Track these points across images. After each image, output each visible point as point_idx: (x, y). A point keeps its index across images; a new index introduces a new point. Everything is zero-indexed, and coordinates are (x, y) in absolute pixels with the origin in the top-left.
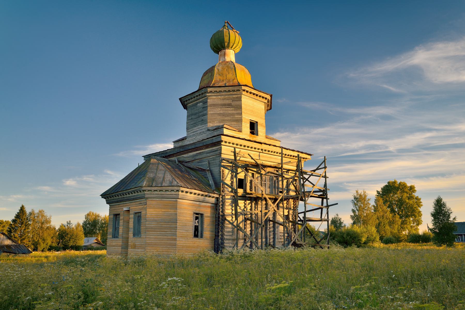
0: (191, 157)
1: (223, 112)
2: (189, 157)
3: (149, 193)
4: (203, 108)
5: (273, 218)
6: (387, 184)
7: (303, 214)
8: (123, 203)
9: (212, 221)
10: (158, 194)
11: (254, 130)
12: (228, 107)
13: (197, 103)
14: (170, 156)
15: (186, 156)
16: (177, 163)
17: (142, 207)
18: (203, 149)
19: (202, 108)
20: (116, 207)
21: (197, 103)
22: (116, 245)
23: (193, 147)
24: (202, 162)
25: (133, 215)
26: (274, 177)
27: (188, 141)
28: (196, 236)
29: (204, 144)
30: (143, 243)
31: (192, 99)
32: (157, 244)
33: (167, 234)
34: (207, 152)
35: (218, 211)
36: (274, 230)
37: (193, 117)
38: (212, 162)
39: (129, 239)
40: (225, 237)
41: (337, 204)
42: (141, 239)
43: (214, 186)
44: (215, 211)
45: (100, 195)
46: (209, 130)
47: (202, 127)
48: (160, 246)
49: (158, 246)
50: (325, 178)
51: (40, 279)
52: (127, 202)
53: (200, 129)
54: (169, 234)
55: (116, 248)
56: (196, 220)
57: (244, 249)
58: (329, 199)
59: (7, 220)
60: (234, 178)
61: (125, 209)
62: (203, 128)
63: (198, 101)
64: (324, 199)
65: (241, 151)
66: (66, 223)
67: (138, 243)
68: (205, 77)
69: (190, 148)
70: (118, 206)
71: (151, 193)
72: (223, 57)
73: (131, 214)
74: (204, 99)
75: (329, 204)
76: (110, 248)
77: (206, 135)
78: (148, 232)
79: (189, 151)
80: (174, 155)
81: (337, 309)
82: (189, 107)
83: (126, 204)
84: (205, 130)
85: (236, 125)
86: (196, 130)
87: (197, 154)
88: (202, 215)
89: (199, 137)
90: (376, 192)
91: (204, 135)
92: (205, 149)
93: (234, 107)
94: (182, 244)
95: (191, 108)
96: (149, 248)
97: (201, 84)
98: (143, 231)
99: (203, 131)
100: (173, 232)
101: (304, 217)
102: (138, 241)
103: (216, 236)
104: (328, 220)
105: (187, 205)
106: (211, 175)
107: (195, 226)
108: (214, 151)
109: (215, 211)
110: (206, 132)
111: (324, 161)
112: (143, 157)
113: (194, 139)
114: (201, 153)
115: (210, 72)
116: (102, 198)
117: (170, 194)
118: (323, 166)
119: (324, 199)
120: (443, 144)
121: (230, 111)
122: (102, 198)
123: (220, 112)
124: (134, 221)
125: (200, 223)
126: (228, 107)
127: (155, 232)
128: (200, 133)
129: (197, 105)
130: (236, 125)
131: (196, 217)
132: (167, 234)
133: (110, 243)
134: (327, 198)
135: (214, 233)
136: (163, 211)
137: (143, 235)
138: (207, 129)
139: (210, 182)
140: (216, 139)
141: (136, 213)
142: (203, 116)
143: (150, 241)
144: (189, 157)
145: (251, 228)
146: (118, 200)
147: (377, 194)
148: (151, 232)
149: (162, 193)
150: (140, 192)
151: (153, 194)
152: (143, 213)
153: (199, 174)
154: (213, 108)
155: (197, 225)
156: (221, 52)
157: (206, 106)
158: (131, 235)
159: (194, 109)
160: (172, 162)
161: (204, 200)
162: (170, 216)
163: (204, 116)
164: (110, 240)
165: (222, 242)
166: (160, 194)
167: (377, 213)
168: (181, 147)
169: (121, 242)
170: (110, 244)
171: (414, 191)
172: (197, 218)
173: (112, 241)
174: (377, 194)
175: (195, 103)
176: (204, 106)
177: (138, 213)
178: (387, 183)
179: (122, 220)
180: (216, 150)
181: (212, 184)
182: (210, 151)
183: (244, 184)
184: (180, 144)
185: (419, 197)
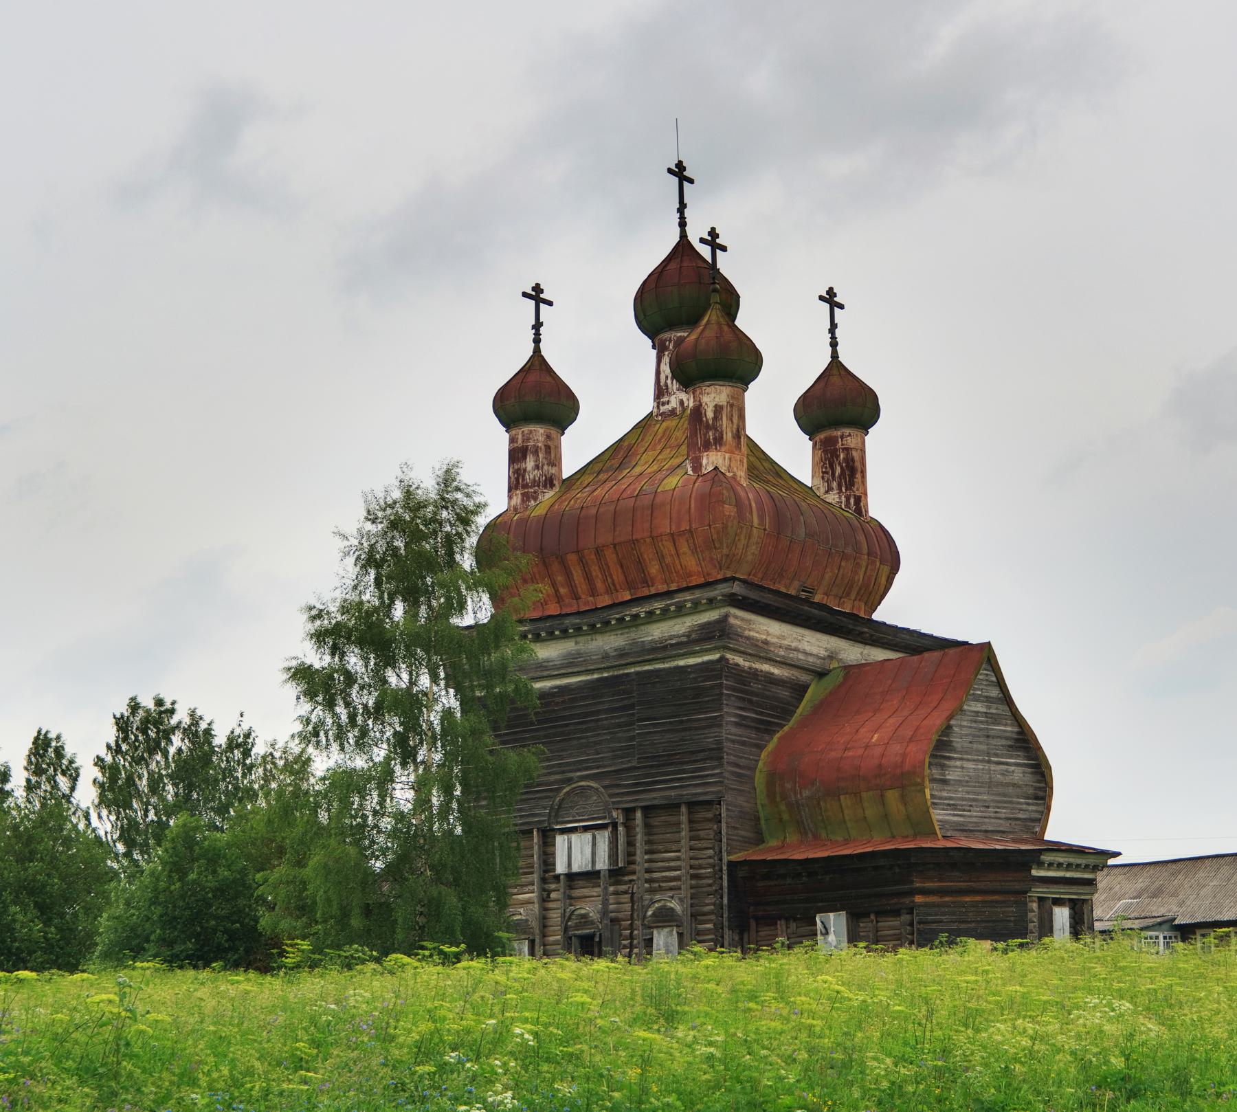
51: (672, 987)
57: (300, 1104)
59: (835, 291)
60: (769, 845)
66: (96, 769)
81: (667, 1111)
82: (548, 437)
90: (292, 690)
105: (575, 898)
114: (770, 722)
120: (924, 846)
121: (1042, 785)
127: (1074, 889)
167: (152, 816)
185: (123, 709)
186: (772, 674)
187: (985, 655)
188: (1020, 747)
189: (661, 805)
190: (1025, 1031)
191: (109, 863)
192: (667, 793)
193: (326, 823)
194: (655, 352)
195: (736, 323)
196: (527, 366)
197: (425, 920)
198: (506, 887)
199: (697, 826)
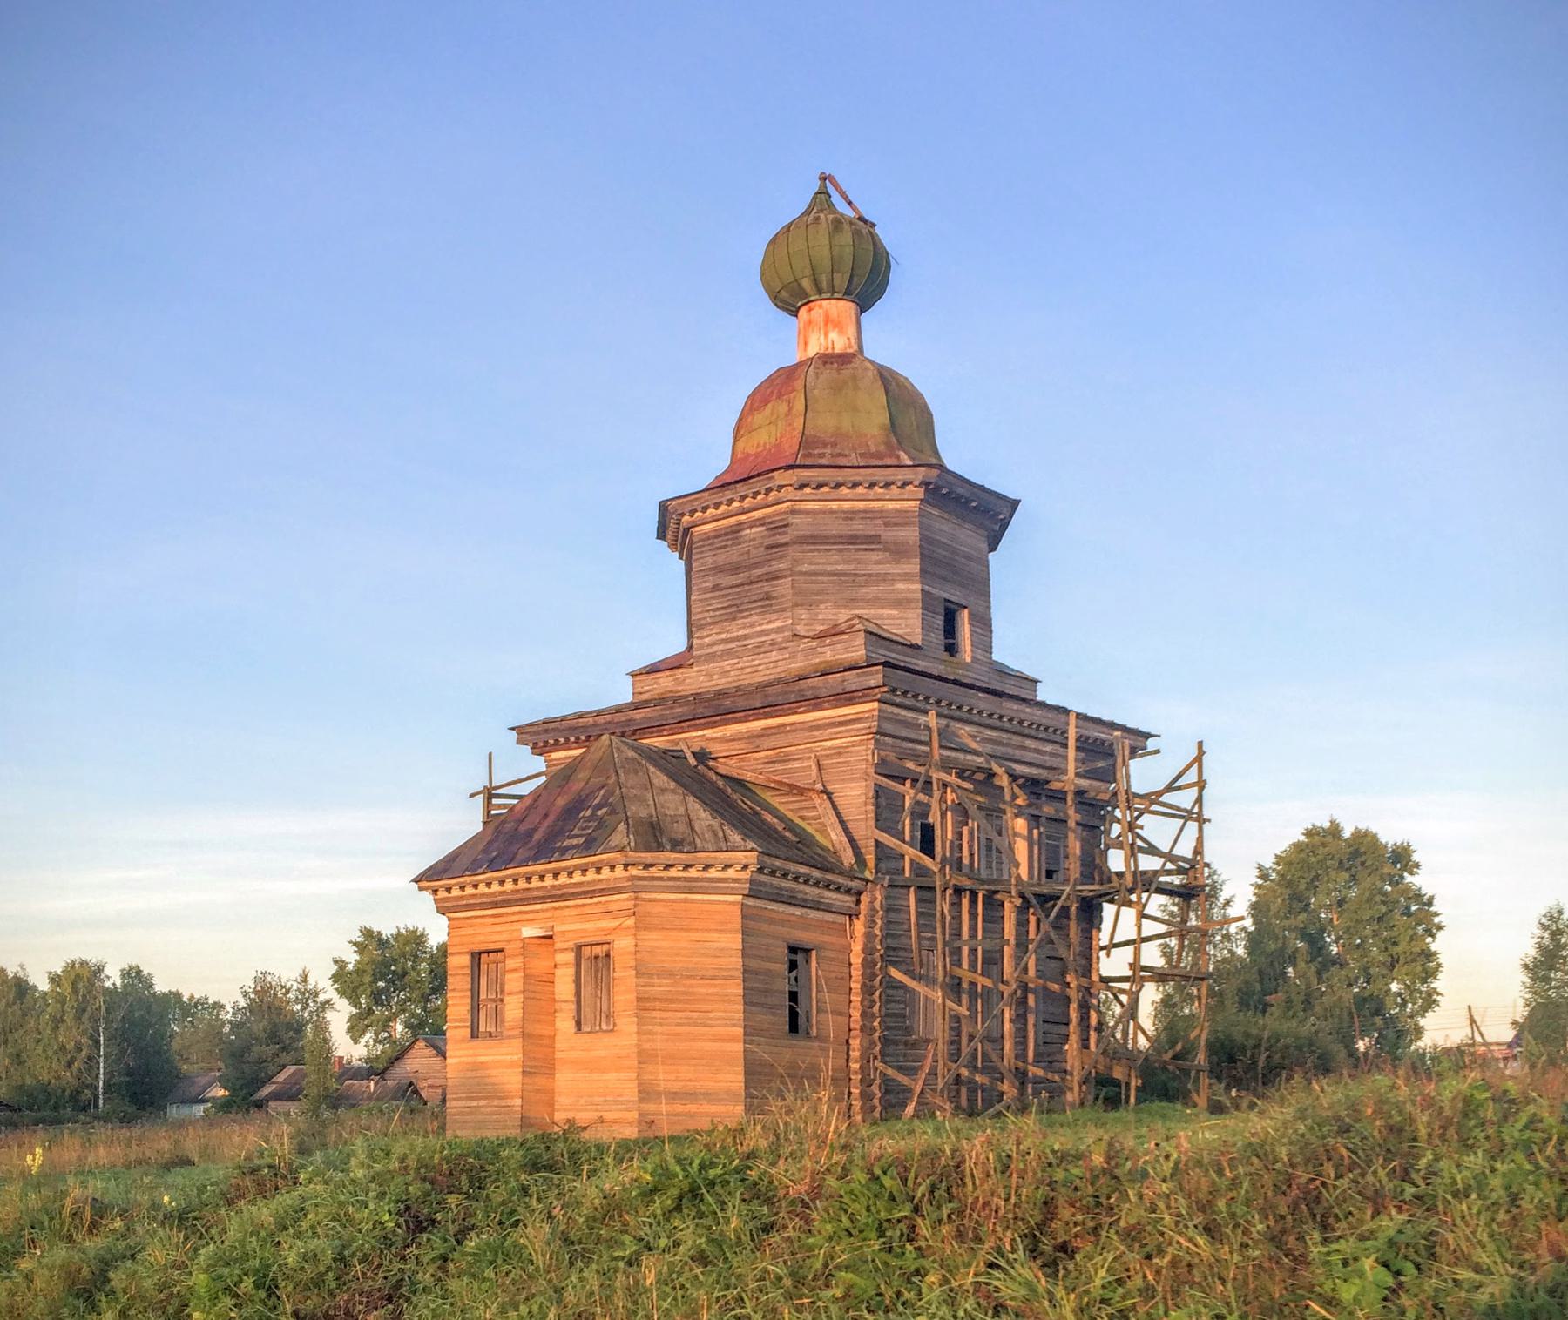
0: (739, 739)
1: (852, 567)
4: (769, 547)
6: (1303, 838)
12: (866, 549)
13: (739, 527)
15: (715, 735)
19: (762, 549)
20: (484, 925)
24: (789, 760)
34: (814, 724)
45: (412, 881)
54: (718, 1019)
56: (790, 972)
61: (528, 932)
63: (743, 518)
68: (758, 418)
72: (822, 332)
79: (736, 718)
80: (664, 730)
85: (898, 622)
87: (769, 732)
90: (1256, 872)
93: (885, 550)
97: (740, 444)
99: (770, 637)
100: (730, 1012)
108: (841, 724)
111: (1199, 759)
112: (514, 732)
118: (1191, 777)
126: (866, 549)
129: (738, 531)
130: (898, 622)
138: (790, 633)
147: (1260, 882)
154: (811, 551)
155: (795, 990)
156: (810, 310)
158: (565, 1024)
168: (661, 701)
171: (1413, 867)
174: (1260, 882)
176: (771, 541)
178: (1303, 834)
180: (851, 717)
181: (841, 842)
182: (827, 721)
184: (665, 683)
186: (814, 837)
187: (879, 823)
188: (714, 1094)
189: (736, 723)
190: (774, 1257)
191: (172, 1026)
193: (1425, 1043)
194: (623, 693)
195: (995, 657)
196: (747, 408)
197: (521, 959)
198: (1279, 884)
199: (891, 926)
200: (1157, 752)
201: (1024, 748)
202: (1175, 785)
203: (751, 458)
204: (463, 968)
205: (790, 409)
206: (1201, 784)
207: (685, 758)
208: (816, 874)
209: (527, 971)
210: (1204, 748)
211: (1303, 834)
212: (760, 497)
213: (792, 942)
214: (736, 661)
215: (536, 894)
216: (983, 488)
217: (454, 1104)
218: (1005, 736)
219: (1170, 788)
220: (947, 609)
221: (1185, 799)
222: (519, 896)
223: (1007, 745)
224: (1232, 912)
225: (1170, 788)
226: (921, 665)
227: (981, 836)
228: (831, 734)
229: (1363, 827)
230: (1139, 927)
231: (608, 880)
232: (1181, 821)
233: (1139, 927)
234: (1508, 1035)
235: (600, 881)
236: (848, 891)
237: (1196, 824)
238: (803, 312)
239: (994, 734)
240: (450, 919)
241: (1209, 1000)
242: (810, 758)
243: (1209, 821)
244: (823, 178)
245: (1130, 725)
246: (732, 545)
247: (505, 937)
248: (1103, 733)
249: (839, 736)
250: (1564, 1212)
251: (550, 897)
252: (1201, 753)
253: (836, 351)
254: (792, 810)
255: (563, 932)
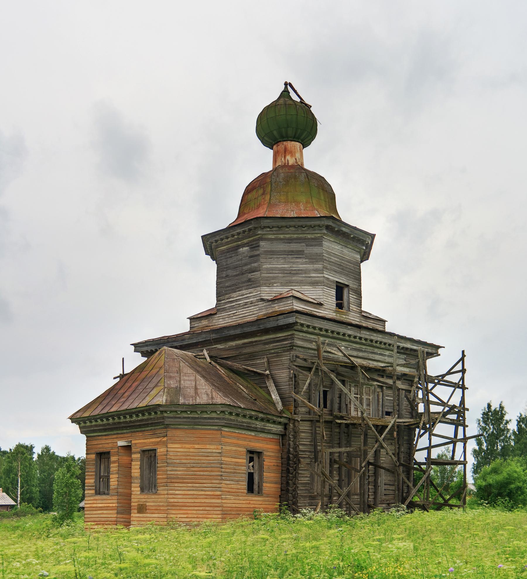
2: (228, 350)
3: (172, 416)
4: (251, 257)
5: (375, 460)
7: (426, 451)
8: (115, 432)
9: (276, 464)
10: (188, 418)
11: (342, 300)
14: (314, 230)
15: (221, 347)
16: (208, 359)
17: (159, 439)
18: (257, 336)
21: (239, 247)
22: (104, 507)
23: (238, 331)
24: (255, 359)
25: (140, 455)
26: (377, 386)
27: (221, 317)
28: (250, 489)
29: (261, 326)
30: (163, 503)
31: (229, 238)
32: (188, 504)
33: (205, 487)
34: (266, 341)
35: (287, 447)
36: (375, 480)
37: (230, 272)
38: (274, 361)
39: (132, 496)
40: (298, 492)
41: (123, 359)
42: (157, 496)
43: (280, 404)
44: (280, 447)
46: (262, 300)
47: (250, 293)
48: (193, 508)
49: (191, 508)
50: (461, 390)
52: (125, 431)
53: (246, 296)
55: (105, 512)
56: (249, 463)
58: (467, 426)
61: (121, 443)
62: (252, 295)
64: (459, 427)
65: (113, 515)
67: (152, 504)
69: (232, 332)
70: (104, 437)
71: (174, 416)
72: (283, 156)
73: (135, 453)
74: (253, 241)
75: (468, 435)
76: (91, 512)
77: (258, 309)
78: (171, 484)
81: (1, 556)
83: (122, 434)
84: (255, 299)
86: (237, 298)
87: (245, 345)
88: (259, 454)
89: (242, 311)
91: (252, 308)
92: (260, 336)
94: (230, 504)
95: (226, 256)
96: (174, 512)
98: (161, 483)
99: (251, 300)
101: (428, 458)
102: (150, 500)
103: (283, 490)
104: (465, 463)
106: (274, 383)
107: (249, 473)
109: (281, 447)
110: (257, 304)
111: (462, 359)
112: (133, 346)
113: (232, 315)
114: (252, 342)
115: (260, 186)
116: (72, 422)
117: (209, 418)
118: (459, 367)
119: (459, 427)
122: (72, 422)
123: (284, 266)
124: (141, 465)
125: (256, 467)
128: (246, 305)
131: (250, 457)
132: (205, 487)
133: (90, 504)
134: (465, 426)
135: (279, 486)
136: (196, 447)
137: (161, 490)
139: (273, 397)
140: (283, 320)
141: (144, 451)
142: (250, 273)
143: (176, 500)
144: (228, 350)
145: (339, 476)
146: (108, 427)
148: (176, 485)
149: (195, 416)
150: (156, 413)
151: (180, 418)
152: (161, 450)
153: (249, 381)
154: (271, 258)
155: (252, 471)
157: (257, 253)
158: (136, 489)
159: (231, 257)
160: (199, 358)
161: (264, 428)
162: (208, 456)
163: (254, 272)
164: (92, 498)
165: (294, 500)
166: (192, 417)
169: (115, 501)
170: (91, 505)
172: (251, 460)
173: (96, 500)
175: (234, 247)
177: (149, 450)
179: (114, 462)
182: (272, 340)
183: (328, 399)
192: (352, 321)
194: (185, 327)
200: (115, 378)
201: (276, 428)
202: (451, 371)
203: (495, 432)
204: (272, 253)
205: (264, 191)
206: (463, 371)
207: (206, 359)
208: (261, 415)
209: (120, 462)
210: (465, 354)
211: (47, 449)
212: (246, 233)
213: (249, 449)
214: (235, 312)
215: (123, 425)
216: (355, 228)
217: (265, 479)
218: (364, 347)
219: (449, 373)
220: (337, 286)
221: (455, 378)
222: (116, 426)
223: (365, 351)
224: (509, 426)
225: (449, 373)
226: (321, 312)
227: (235, 296)
228: (274, 346)
229: (47, 445)
230: (430, 440)
231: (154, 418)
232: (453, 389)
233: (430, 440)
234: (269, 153)
235: (151, 419)
236: (280, 423)
237: (461, 390)
238: (275, 147)
239: (358, 346)
240: (87, 437)
241: (337, 455)
242: (264, 358)
243: (467, 388)
244: (286, 84)
245: (416, 338)
246: (239, 283)
247: (110, 445)
248: (415, 346)
249: (195, 496)
250: (1, 573)
251: (129, 426)
252: (464, 355)
253: (290, 164)
254: (256, 383)
255: (136, 444)
